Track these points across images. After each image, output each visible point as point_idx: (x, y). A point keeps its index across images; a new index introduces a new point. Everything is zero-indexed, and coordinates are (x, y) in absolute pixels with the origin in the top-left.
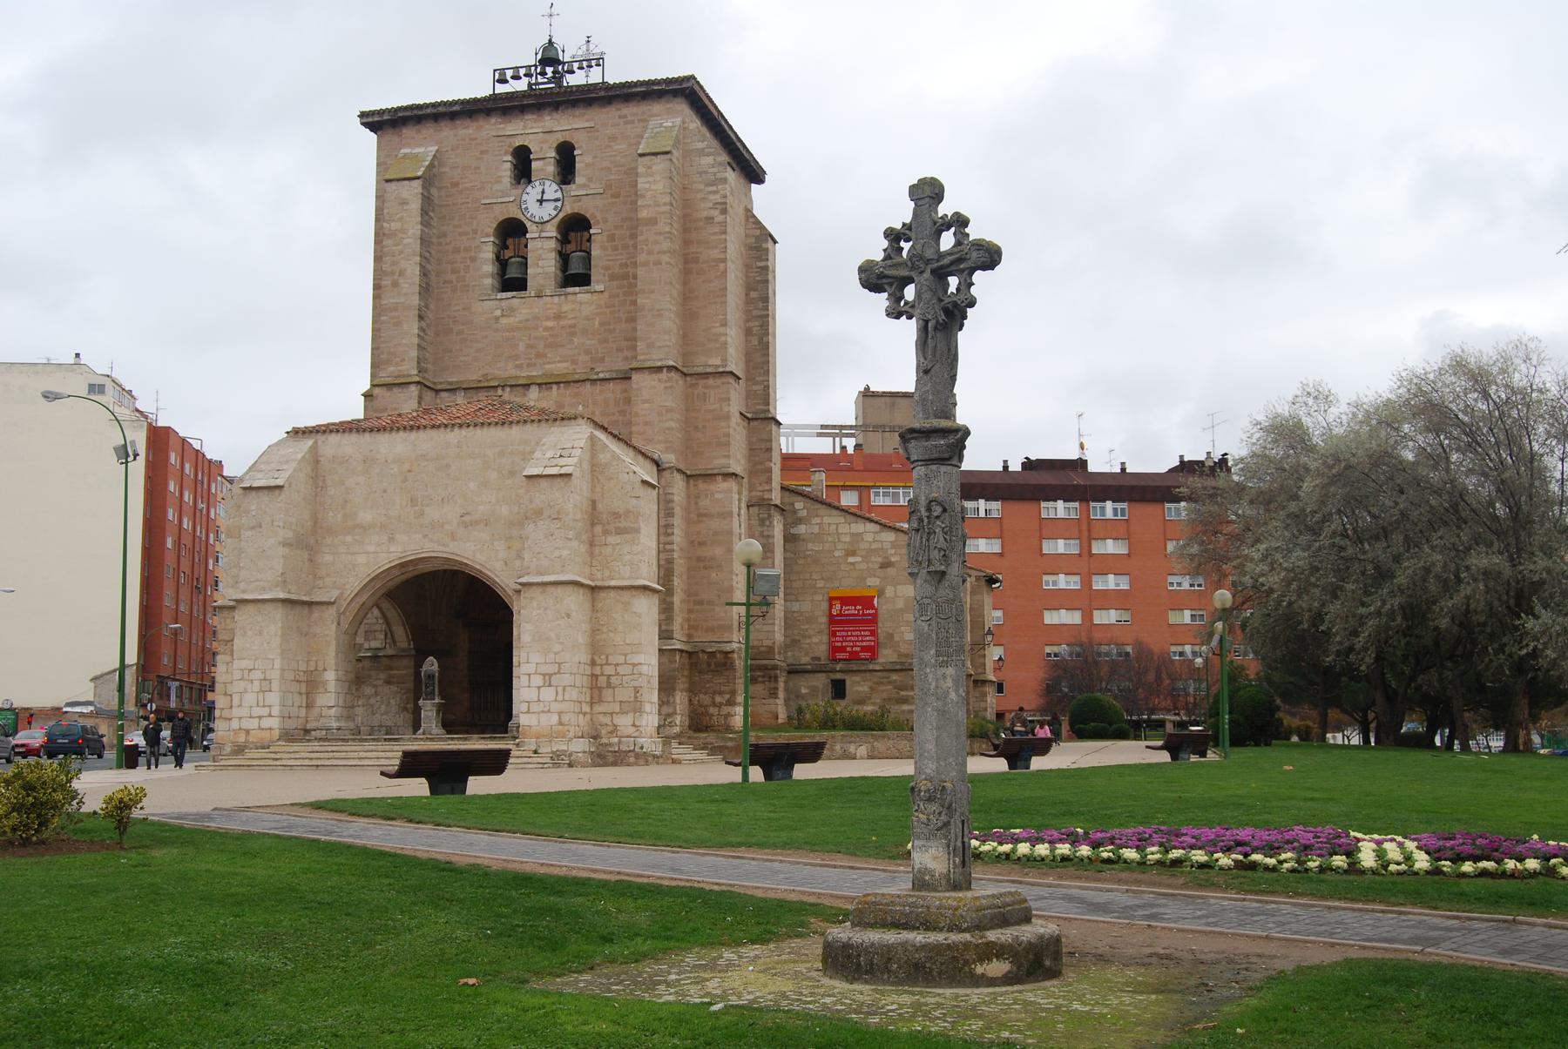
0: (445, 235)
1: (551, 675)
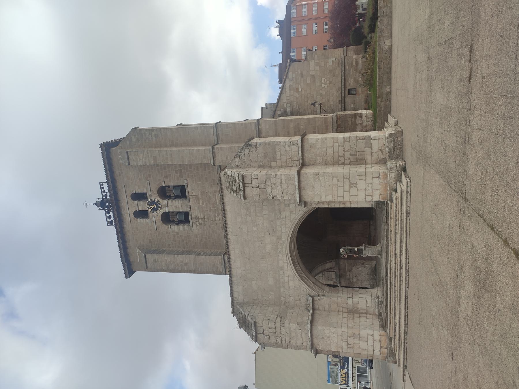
0: (169, 245)
1: (351, 184)
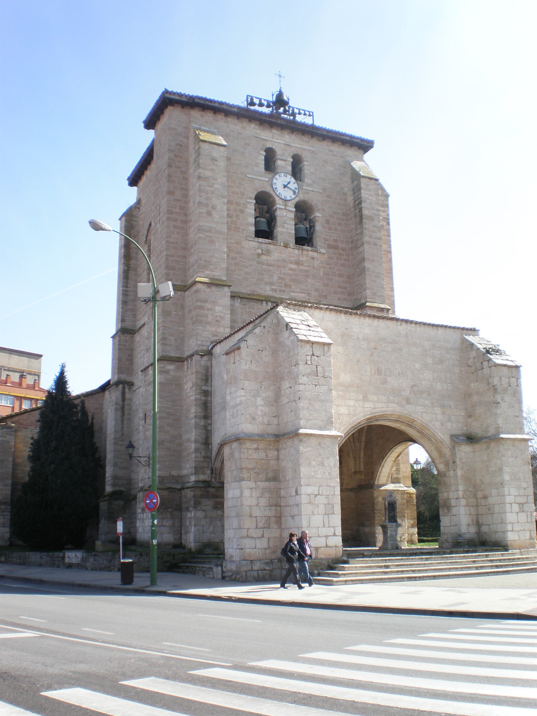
1: (523, 504)
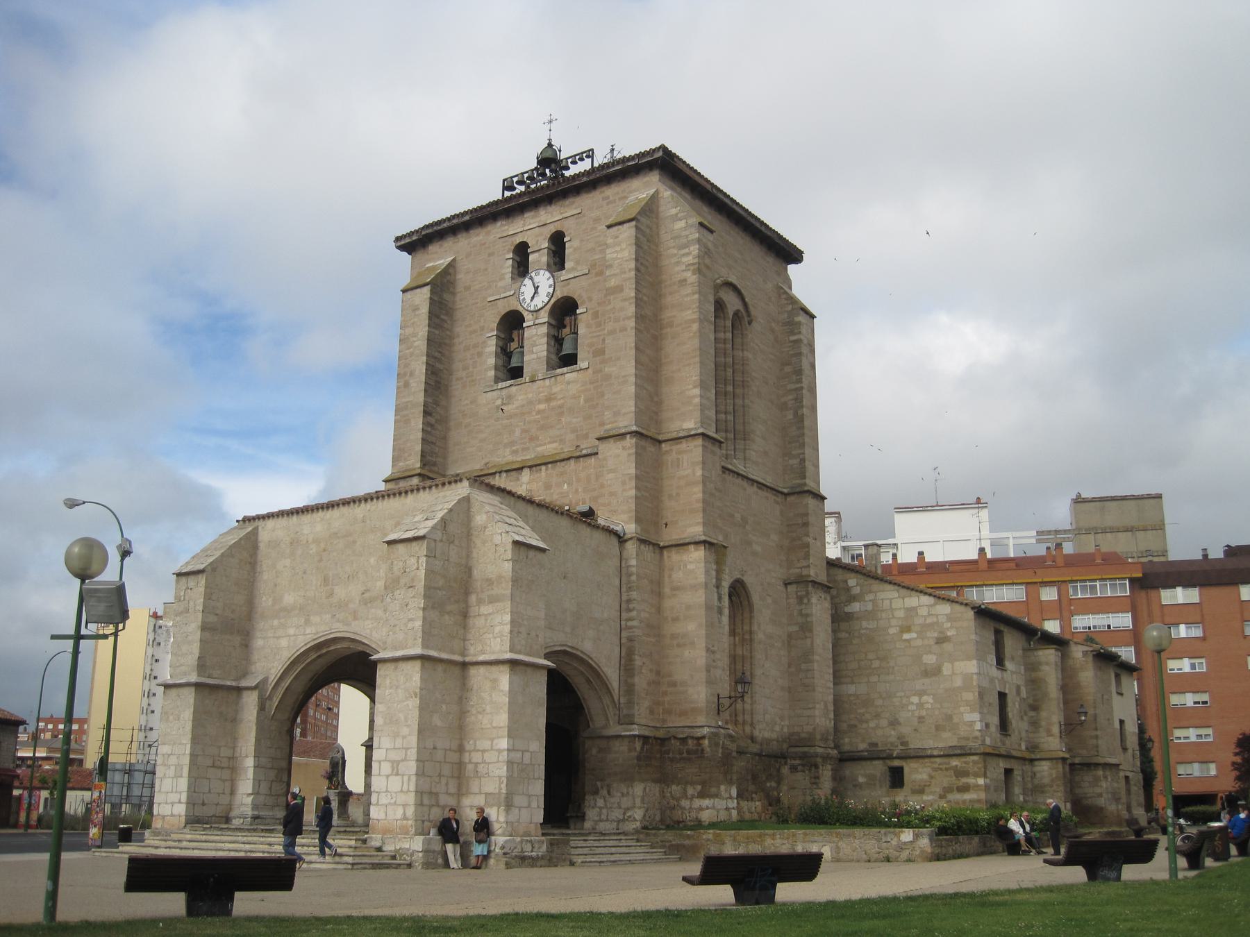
1: (398, 762)
